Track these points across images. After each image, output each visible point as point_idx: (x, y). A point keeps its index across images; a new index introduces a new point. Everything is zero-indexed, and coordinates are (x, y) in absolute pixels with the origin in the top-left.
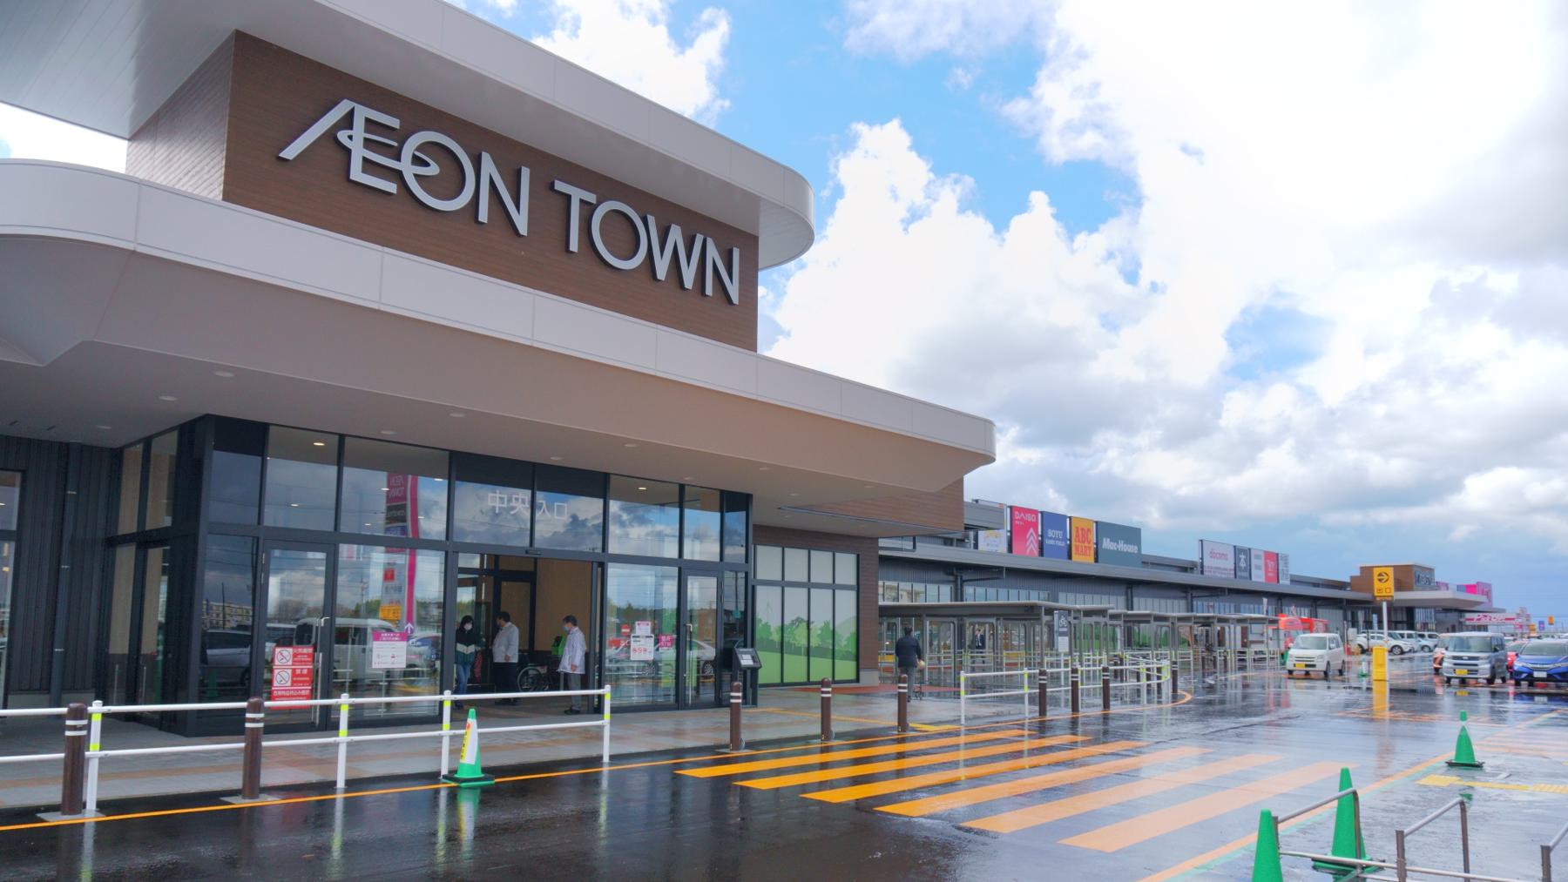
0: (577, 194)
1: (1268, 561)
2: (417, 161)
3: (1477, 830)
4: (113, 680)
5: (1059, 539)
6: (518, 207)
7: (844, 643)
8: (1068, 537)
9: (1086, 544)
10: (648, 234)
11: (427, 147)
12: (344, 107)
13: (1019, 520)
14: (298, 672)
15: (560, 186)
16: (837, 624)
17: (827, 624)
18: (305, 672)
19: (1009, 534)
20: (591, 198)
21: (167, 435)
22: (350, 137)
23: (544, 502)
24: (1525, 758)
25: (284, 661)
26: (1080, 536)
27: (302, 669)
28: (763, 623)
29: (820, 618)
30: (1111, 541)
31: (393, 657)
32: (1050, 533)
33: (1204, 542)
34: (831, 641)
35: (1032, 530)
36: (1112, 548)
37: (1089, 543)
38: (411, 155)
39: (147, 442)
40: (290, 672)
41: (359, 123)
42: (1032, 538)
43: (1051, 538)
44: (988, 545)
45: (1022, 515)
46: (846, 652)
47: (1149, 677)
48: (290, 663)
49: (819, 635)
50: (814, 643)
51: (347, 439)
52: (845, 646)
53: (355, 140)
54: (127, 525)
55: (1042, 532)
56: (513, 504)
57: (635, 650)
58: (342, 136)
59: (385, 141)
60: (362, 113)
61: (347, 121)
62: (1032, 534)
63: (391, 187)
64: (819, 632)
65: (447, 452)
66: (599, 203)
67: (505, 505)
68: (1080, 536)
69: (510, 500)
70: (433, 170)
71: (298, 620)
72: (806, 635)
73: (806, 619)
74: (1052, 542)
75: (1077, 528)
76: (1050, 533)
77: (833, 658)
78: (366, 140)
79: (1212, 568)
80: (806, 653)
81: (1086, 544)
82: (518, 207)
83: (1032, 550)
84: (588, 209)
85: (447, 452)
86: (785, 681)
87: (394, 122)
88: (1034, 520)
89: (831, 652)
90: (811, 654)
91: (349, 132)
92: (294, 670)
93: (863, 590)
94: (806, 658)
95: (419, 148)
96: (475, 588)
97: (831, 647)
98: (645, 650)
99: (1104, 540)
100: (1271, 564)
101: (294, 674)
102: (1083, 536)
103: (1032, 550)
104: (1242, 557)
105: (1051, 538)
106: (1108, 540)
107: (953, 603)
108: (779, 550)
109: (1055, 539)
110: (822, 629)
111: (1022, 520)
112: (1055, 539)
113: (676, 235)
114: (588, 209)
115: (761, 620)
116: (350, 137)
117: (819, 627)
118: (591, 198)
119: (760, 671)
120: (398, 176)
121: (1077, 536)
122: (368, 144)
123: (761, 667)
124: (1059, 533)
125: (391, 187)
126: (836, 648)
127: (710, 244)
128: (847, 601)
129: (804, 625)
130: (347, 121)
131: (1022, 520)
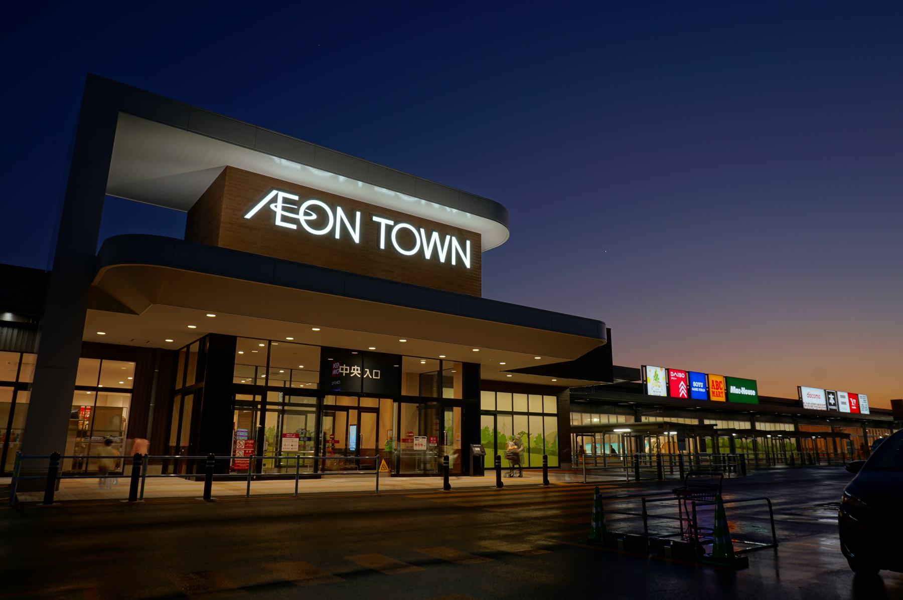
0: (384, 222)
1: (851, 399)
2: (306, 214)
3: (791, 583)
4: (777, 500)
5: (701, 388)
6: (354, 228)
7: (550, 446)
8: (707, 386)
9: (719, 390)
10: (420, 236)
11: (313, 208)
12: (274, 193)
13: (673, 377)
14: (247, 452)
15: (375, 219)
16: (545, 435)
17: (540, 435)
18: (250, 452)
19: (668, 385)
20: (391, 223)
21: (191, 342)
22: (276, 206)
23: (368, 370)
24: (633, 512)
25: (241, 446)
26: (715, 385)
27: (249, 450)
28: (501, 434)
29: (536, 431)
30: (736, 388)
31: (292, 446)
32: (695, 384)
33: (690, 374)
34: (542, 445)
35: (682, 383)
36: (737, 393)
37: (721, 389)
38: (304, 210)
39: (188, 346)
40: (243, 451)
41: (280, 200)
42: (682, 387)
43: (696, 387)
44: (654, 392)
45: (675, 373)
46: (552, 451)
47: (725, 467)
48: (243, 447)
49: (535, 441)
50: (531, 446)
51: (443, 361)
52: (551, 447)
53: (278, 209)
54: (179, 386)
55: (689, 383)
56: (352, 371)
57: (416, 444)
58: (272, 206)
59: (291, 207)
60: (282, 195)
61: (274, 200)
62: (682, 385)
63: (294, 227)
64: (535, 439)
65: (439, 361)
66: (396, 224)
67: (348, 372)
68: (715, 385)
69: (350, 369)
70: (314, 217)
71: (391, 438)
72: (528, 441)
73: (527, 432)
74: (696, 389)
75: (713, 381)
76: (695, 384)
77: (529, 452)
78: (283, 207)
79: (809, 403)
80: (528, 451)
81: (719, 390)
82: (354, 228)
83: (683, 394)
84: (389, 229)
85: (439, 361)
86: (531, 466)
87: (296, 198)
88: (683, 377)
89: (543, 451)
90: (9, 407)
91: (275, 204)
92: (245, 451)
93: (562, 417)
94: (528, 454)
95: (308, 208)
96: (498, 415)
97: (542, 448)
98: (422, 445)
99: (732, 387)
100: (854, 401)
101: (245, 453)
102: (717, 385)
103: (683, 394)
104: (831, 396)
105: (696, 387)
106: (744, 388)
107: (636, 423)
108: (526, 395)
109: (698, 387)
110: (536, 438)
111: (675, 376)
112: (698, 387)
113: (435, 236)
114: (389, 229)
115: (500, 433)
116: (276, 206)
117: (535, 437)
118: (391, 223)
119: (485, 457)
120: (296, 221)
121: (713, 385)
122: (284, 209)
123: (485, 455)
124: (701, 384)
125: (294, 227)
126: (546, 448)
127: (454, 239)
128: (552, 423)
129: (526, 436)
130: (274, 200)
131: (675, 376)
